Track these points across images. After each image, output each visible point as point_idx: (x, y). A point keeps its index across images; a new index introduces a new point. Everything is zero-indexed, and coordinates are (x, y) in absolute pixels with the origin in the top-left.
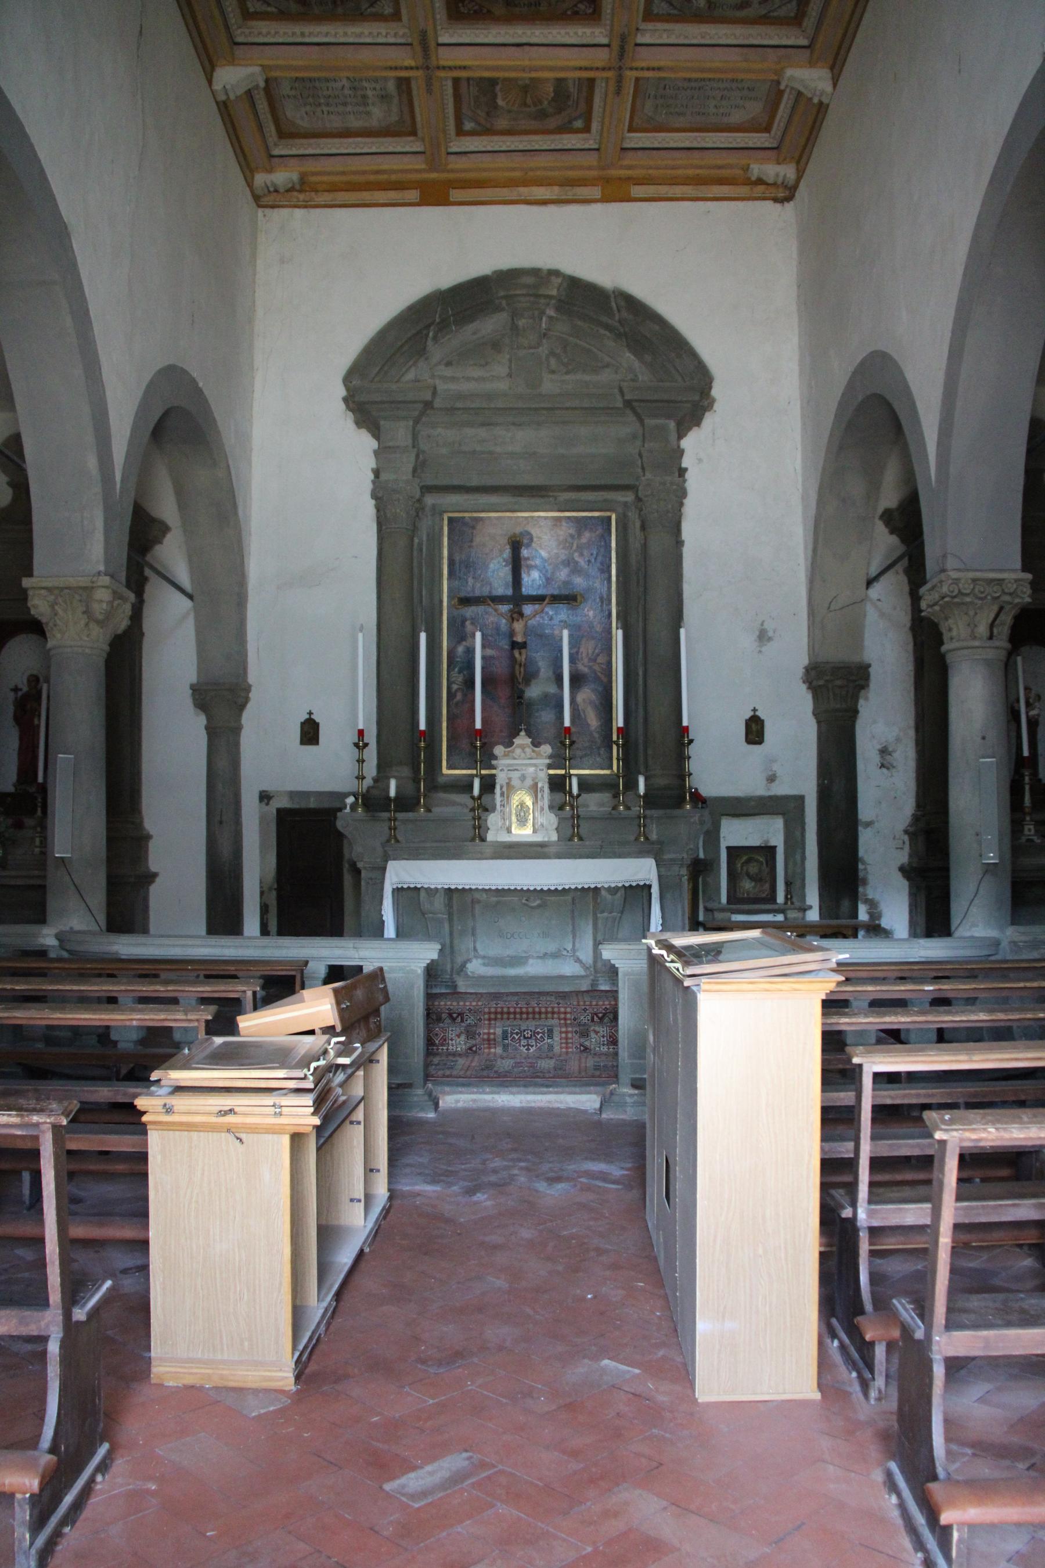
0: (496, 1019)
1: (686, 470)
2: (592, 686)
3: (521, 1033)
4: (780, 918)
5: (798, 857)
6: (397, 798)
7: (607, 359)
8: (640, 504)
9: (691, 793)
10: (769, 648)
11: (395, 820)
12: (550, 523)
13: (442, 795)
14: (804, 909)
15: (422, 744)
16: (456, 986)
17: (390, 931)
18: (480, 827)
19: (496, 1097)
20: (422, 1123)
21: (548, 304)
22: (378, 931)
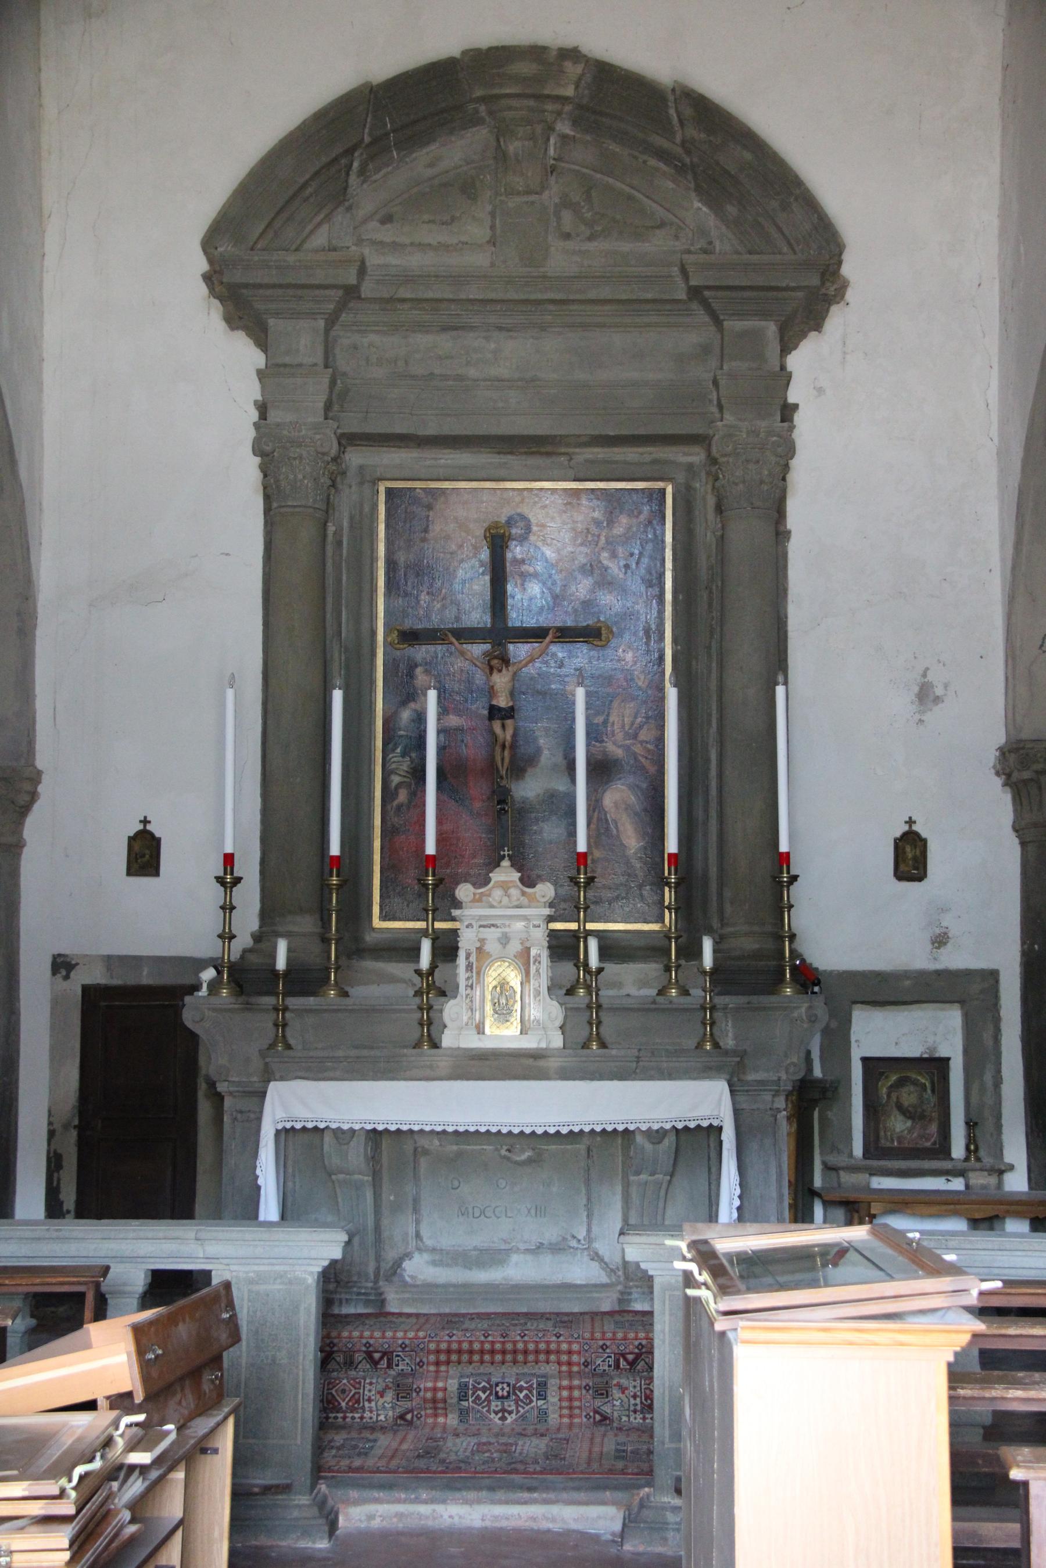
0: (448, 1363)
1: (795, 407)
2: (631, 779)
3: (491, 1388)
4: (957, 1184)
5: (988, 1078)
6: (288, 972)
7: (660, 212)
8: (714, 469)
9: (794, 969)
10: (935, 716)
11: (285, 1009)
13: (369, 964)
14: (1000, 1171)
15: (335, 880)
16: (383, 1302)
17: (269, 1208)
18: (430, 1023)
19: (440, 1508)
21: (559, 113)
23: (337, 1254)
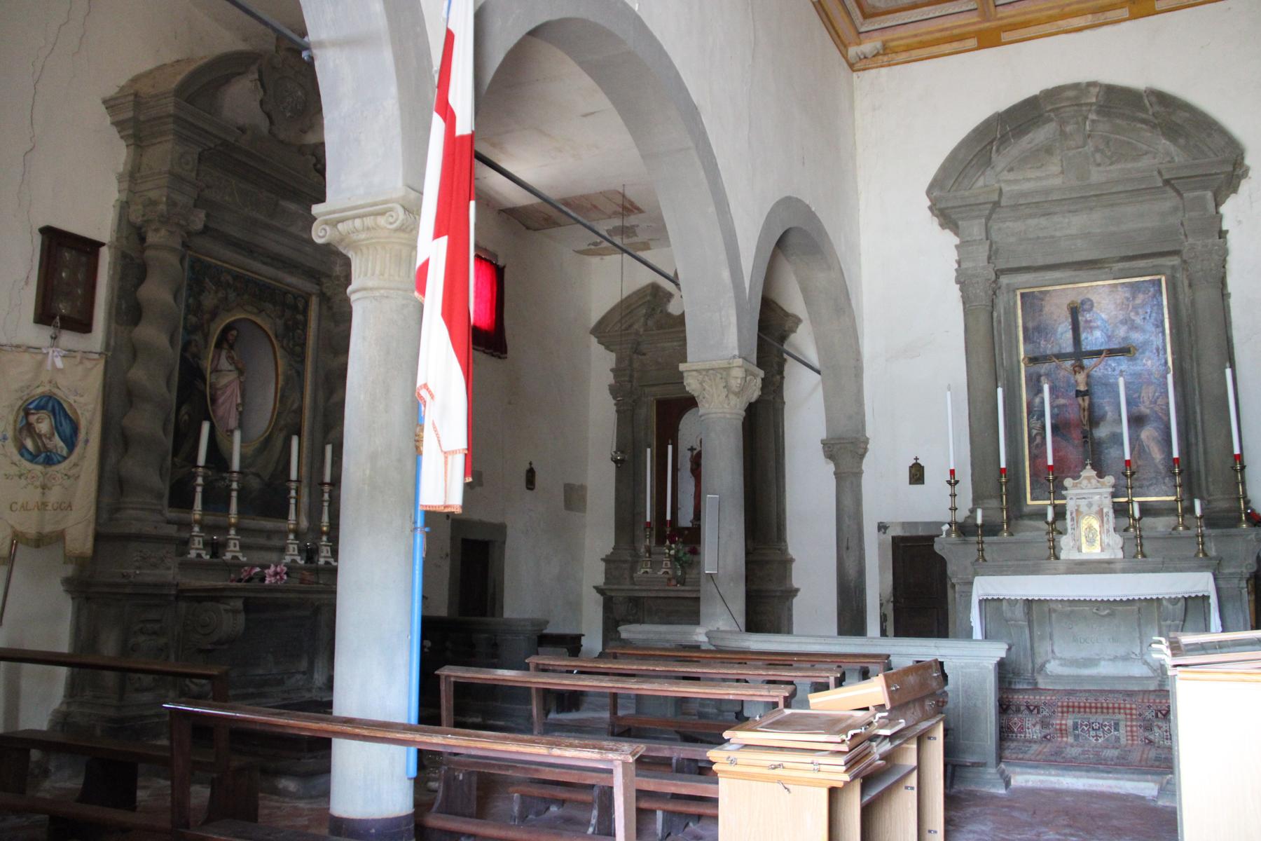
1: (1227, 232)
2: (1155, 424)
3: (1090, 725)
6: (983, 525)
7: (1145, 147)
9: (1247, 515)
12: (1107, 290)
17: (977, 633)
18: (1054, 548)
19: (1061, 779)
20: (994, 797)
22: (968, 634)
23: (1003, 655)
